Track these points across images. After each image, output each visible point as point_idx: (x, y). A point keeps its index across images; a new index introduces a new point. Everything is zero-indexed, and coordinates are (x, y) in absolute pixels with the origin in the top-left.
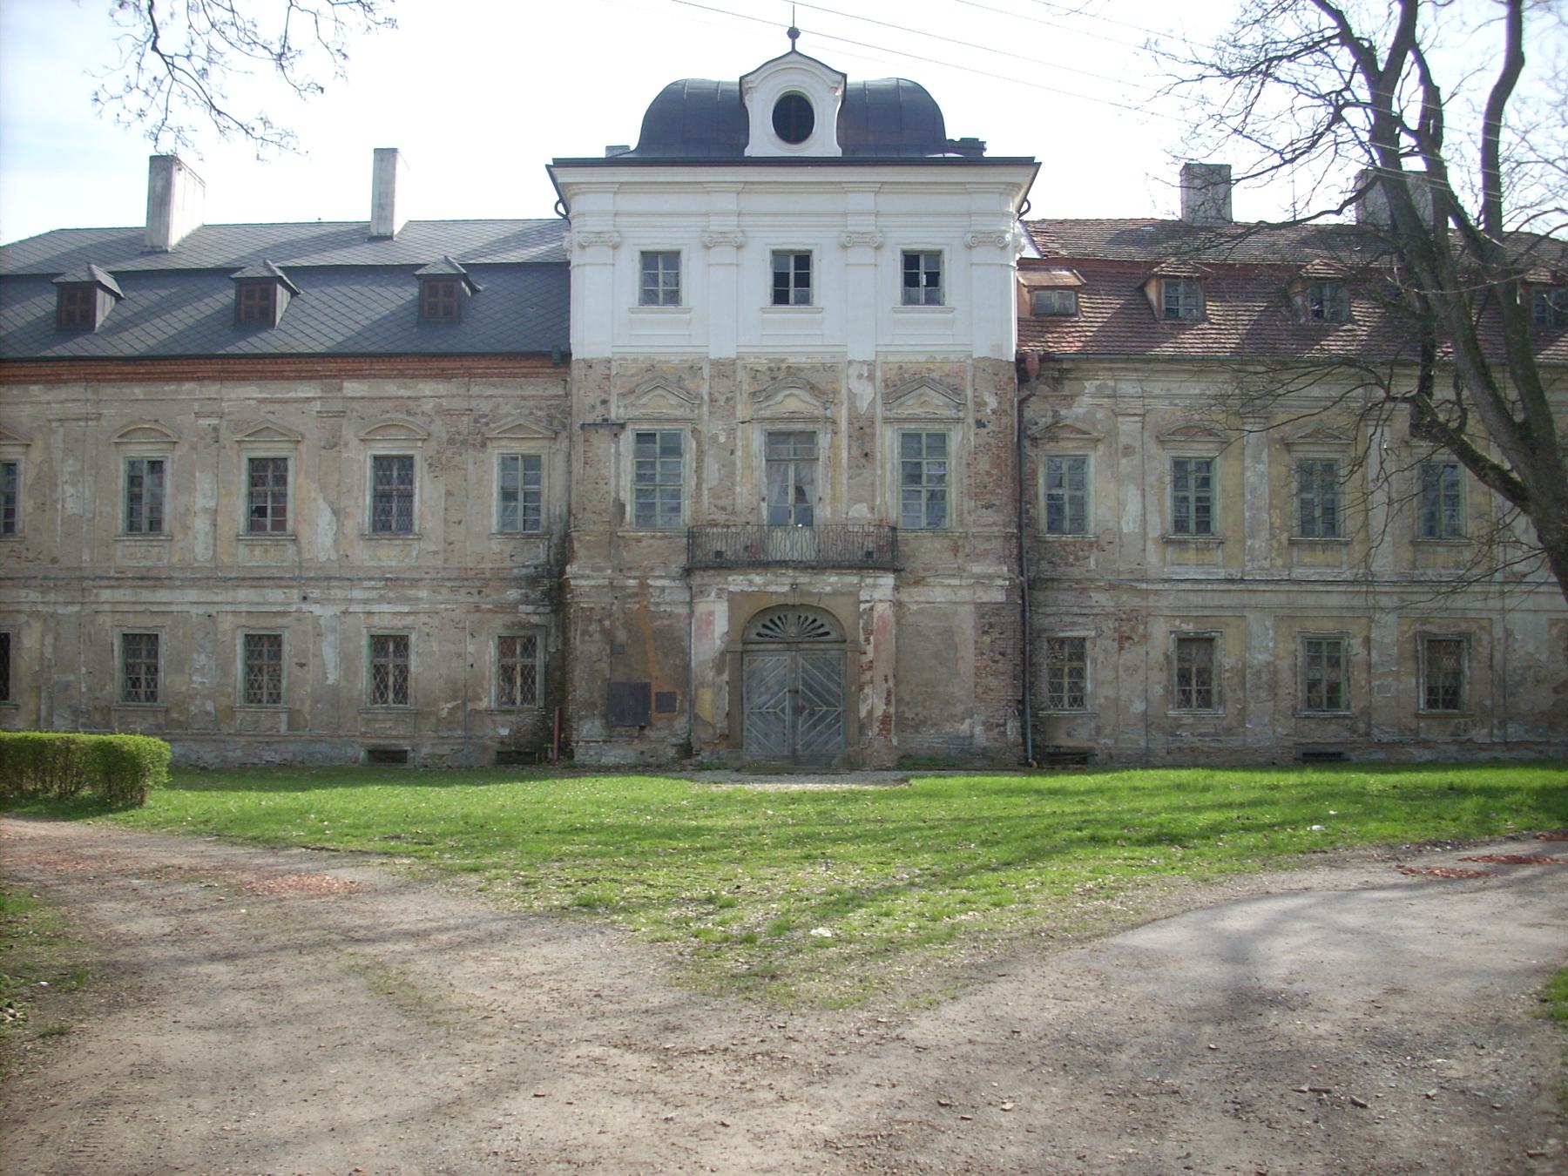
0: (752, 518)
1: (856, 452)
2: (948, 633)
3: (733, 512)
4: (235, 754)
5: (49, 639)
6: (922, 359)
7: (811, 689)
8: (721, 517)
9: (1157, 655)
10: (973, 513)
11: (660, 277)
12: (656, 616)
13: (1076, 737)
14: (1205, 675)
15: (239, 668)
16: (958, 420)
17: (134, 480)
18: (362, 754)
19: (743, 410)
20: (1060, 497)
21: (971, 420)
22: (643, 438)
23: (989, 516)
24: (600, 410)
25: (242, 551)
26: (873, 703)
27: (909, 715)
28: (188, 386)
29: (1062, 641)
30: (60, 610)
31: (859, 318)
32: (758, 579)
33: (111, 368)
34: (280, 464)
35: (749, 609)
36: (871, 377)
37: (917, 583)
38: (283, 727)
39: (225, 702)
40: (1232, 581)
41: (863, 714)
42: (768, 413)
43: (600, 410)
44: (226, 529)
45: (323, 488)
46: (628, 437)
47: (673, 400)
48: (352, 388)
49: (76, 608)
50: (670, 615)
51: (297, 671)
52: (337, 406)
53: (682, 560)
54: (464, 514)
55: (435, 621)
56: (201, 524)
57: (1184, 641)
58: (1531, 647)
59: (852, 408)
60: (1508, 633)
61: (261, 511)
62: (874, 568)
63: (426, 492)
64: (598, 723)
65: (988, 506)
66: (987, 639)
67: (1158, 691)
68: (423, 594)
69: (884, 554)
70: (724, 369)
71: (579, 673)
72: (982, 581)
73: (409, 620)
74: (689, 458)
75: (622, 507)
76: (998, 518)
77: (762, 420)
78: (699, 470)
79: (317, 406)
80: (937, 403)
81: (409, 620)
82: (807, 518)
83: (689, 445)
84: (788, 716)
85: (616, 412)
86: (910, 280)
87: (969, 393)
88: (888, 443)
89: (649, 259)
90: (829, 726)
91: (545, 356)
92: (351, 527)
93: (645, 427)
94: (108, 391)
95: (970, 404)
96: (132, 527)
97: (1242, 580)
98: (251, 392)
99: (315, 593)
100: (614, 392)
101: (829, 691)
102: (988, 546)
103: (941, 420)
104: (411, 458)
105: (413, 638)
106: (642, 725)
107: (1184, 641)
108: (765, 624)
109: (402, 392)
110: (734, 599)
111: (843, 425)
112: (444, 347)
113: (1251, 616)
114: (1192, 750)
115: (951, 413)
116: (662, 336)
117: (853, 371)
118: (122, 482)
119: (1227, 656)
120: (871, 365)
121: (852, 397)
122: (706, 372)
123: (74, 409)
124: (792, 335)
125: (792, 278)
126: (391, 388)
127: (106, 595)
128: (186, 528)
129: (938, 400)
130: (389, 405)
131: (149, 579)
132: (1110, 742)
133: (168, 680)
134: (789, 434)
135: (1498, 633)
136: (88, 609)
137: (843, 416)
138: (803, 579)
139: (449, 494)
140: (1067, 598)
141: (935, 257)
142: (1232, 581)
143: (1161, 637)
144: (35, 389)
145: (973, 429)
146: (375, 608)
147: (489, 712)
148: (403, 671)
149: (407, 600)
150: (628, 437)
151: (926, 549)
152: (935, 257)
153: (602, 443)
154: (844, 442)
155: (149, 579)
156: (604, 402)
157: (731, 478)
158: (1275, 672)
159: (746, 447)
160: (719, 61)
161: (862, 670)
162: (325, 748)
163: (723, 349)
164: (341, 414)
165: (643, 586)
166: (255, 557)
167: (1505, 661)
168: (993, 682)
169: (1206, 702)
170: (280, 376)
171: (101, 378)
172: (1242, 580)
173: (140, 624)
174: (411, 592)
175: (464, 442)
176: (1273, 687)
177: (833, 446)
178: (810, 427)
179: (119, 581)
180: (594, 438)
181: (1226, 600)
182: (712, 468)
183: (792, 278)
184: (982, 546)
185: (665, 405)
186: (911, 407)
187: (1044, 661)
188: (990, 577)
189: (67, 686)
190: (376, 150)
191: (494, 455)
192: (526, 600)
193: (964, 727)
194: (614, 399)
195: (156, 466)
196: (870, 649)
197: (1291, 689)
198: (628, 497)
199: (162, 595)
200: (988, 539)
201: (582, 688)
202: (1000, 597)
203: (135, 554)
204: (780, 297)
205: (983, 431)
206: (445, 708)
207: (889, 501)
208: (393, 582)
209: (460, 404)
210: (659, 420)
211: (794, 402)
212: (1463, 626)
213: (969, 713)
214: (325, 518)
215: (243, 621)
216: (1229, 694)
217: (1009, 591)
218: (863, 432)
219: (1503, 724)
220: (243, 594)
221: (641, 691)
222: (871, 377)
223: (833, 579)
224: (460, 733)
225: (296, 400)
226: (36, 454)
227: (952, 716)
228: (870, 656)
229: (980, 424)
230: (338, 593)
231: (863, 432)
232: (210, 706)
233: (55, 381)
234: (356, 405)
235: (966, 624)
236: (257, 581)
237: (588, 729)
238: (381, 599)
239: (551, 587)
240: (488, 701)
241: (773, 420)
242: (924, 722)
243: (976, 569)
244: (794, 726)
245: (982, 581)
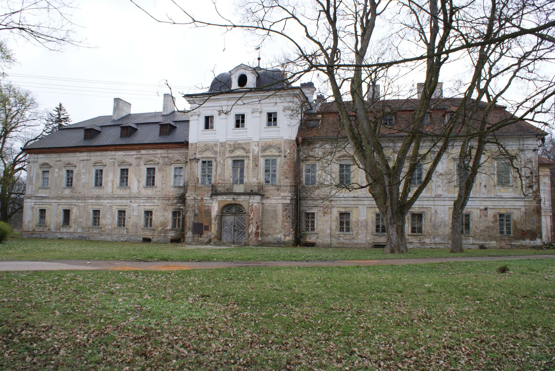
0: (229, 182)
1: (254, 165)
2: (275, 211)
3: (224, 180)
4: (115, 239)
5: (78, 211)
6: (271, 140)
7: (238, 225)
8: (221, 182)
9: (334, 218)
10: (284, 180)
11: (208, 122)
12: (205, 206)
13: (311, 239)
14: (348, 223)
15: (116, 218)
16: (279, 156)
17: (97, 174)
18: (141, 239)
19: (227, 155)
20: (343, 175)
21: (283, 156)
22: (204, 162)
23: (287, 181)
24: (194, 156)
25: (118, 190)
26: (252, 229)
27: (265, 232)
28: (109, 152)
29: (309, 213)
30: (80, 204)
31: (256, 130)
32: (225, 197)
33: (92, 148)
34: (127, 170)
35: (222, 205)
36: (258, 145)
37: (268, 198)
38: (125, 232)
39: (113, 226)
40: (355, 197)
41: (250, 232)
42: (232, 155)
43: (194, 156)
44: (115, 186)
45: (136, 176)
46: (200, 162)
47: (211, 153)
48: (143, 152)
49: (83, 204)
50: (209, 206)
51: (129, 219)
52: (139, 156)
53: (210, 193)
54: (167, 182)
55: (159, 207)
56: (110, 184)
57: (341, 214)
58: (443, 216)
59: (253, 153)
60: (436, 212)
61: (123, 181)
62: (253, 194)
63: (158, 176)
64: (191, 233)
65: (287, 178)
66: (285, 213)
67: (334, 227)
68: (156, 201)
69: (259, 192)
70: (223, 145)
71: (187, 219)
72: (284, 198)
73: (153, 207)
74: (214, 167)
75: (198, 179)
76: (289, 181)
77: (231, 157)
78: (216, 170)
79: (135, 156)
80: (275, 152)
81: (153, 207)
82: (242, 182)
83: (214, 164)
84: (232, 232)
85: (198, 156)
86: (269, 120)
87: (283, 149)
88: (262, 162)
89: (270, 115)
90: (243, 235)
91: (183, 143)
92: (115, 186)
93: (204, 160)
94: (92, 154)
95: (283, 152)
96: (96, 185)
97: (357, 197)
98: (121, 153)
99: (133, 201)
100: (197, 151)
101: (243, 226)
102: (286, 188)
103: (275, 156)
104: (155, 168)
105: (153, 212)
106: (201, 234)
107: (341, 214)
108: (227, 208)
109: (154, 153)
110: (219, 202)
111: (251, 158)
112: (131, 143)
113: (360, 207)
114: (343, 243)
115: (277, 154)
116: (208, 137)
117: (254, 144)
118: (94, 175)
119: (353, 218)
120: (258, 142)
121: (253, 150)
122: (219, 145)
123: (86, 158)
124: (239, 135)
125: (240, 121)
126: (151, 152)
127: (90, 201)
128: (107, 185)
129: (275, 151)
130: (151, 156)
131: (98, 198)
132: (321, 241)
133: (102, 221)
134: (239, 160)
135: (433, 212)
136: (86, 204)
137: (251, 155)
138: (235, 197)
139: (163, 177)
140: (310, 202)
141: (275, 113)
142: (355, 197)
143: (335, 213)
144: (78, 153)
145: (283, 158)
146: (146, 204)
147: (170, 230)
148: (151, 219)
149: (153, 202)
150: (200, 162)
151: (270, 189)
152: (275, 113)
153: (194, 164)
154: (251, 162)
155: (98, 198)
156: (195, 154)
157: (224, 173)
158: (367, 222)
159: (227, 164)
160: (224, 68)
161: (249, 220)
162: (133, 237)
163: (223, 140)
164: (140, 158)
165: (202, 199)
166: (120, 192)
167: (435, 220)
168: (286, 224)
169: (348, 230)
170: (127, 150)
171: (61, 152)
172: (357, 197)
173: (96, 208)
174: (153, 201)
175: (166, 164)
176: (366, 226)
177: (249, 164)
178: (243, 159)
179: (92, 198)
180: (193, 163)
181: (353, 203)
182: (219, 169)
183: (240, 121)
184: (285, 188)
185: (209, 154)
186: (268, 153)
187: (303, 218)
188: (286, 197)
189: (81, 222)
190: (115, 99)
191: (173, 167)
192: (178, 202)
193: (279, 236)
194: (197, 153)
195: (101, 171)
196: (252, 215)
197: (372, 227)
198: (200, 177)
199: (101, 201)
200: (286, 186)
201: (189, 223)
202: (289, 202)
203: (97, 192)
204: (237, 126)
205: (286, 158)
206: (160, 228)
207: (262, 177)
208: (149, 198)
209: (166, 155)
210: (207, 158)
211: (239, 153)
212: (422, 210)
213: (280, 232)
214: (136, 183)
215: (118, 207)
216: (354, 228)
217: (291, 200)
218: (256, 159)
219: (434, 238)
220: (118, 201)
221: (201, 225)
222: (258, 145)
223: (243, 197)
224: (163, 235)
225: (131, 155)
226: (77, 169)
227: (276, 233)
228: (252, 217)
229: (285, 157)
230: (138, 201)
231: (256, 159)
232: (110, 227)
233: (81, 152)
234: (144, 156)
235: (280, 209)
236: (121, 198)
237: (189, 234)
238: (147, 202)
239: (182, 199)
240: (169, 227)
241: (234, 157)
242: (269, 234)
243: (282, 194)
244: (234, 235)
245: (284, 198)
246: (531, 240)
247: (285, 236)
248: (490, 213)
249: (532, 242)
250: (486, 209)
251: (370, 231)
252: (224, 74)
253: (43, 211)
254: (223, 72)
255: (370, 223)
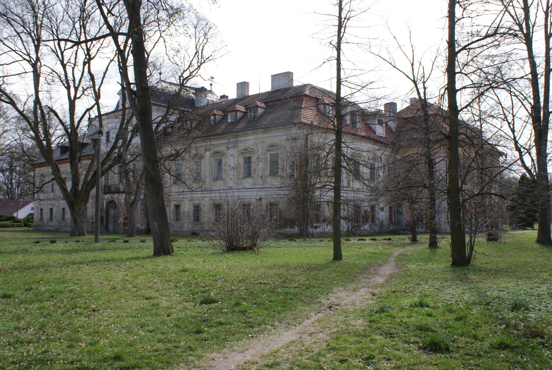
176: (189, 216)
246: (291, 228)
247: (142, 225)
248: (264, 202)
249: (291, 230)
250: (261, 199)
251: (191, 221)
252: (449, 4)
253: (41, 210)
254: (448, 5)
255: (191, 214)
